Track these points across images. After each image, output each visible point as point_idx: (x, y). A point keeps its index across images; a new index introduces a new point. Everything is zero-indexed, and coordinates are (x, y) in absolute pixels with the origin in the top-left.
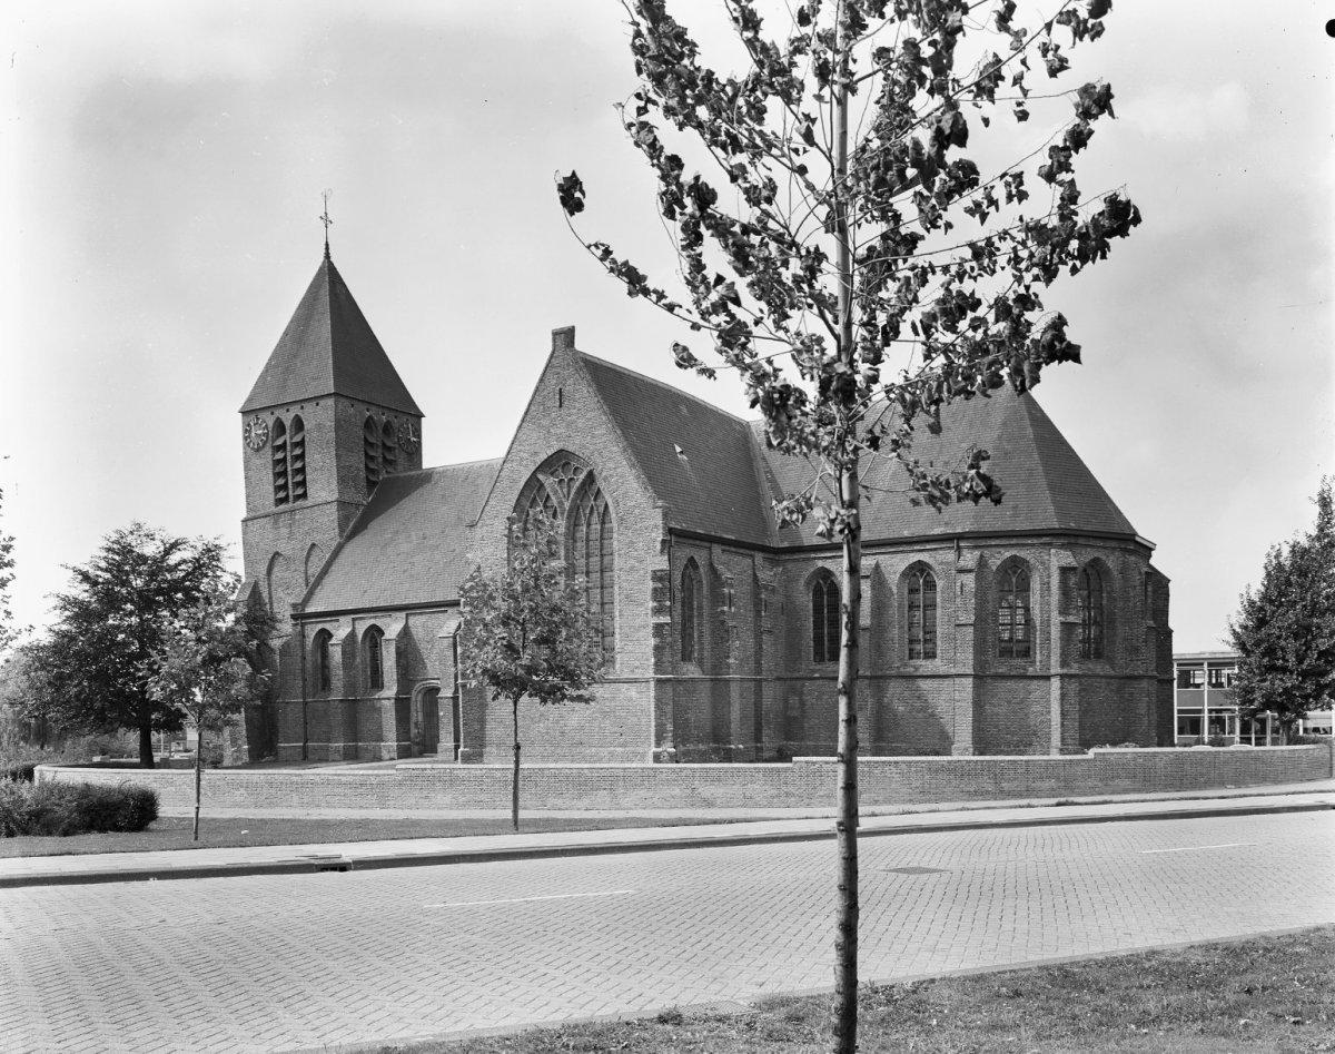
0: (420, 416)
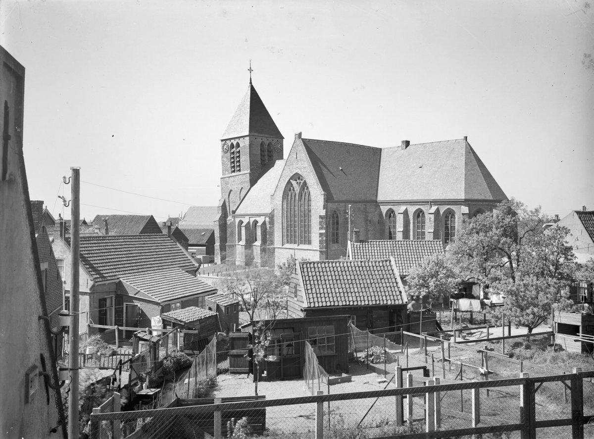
0: (283, 138)
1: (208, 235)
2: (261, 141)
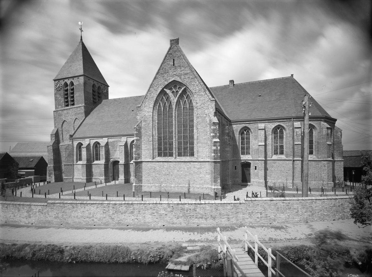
2: (93, 83)
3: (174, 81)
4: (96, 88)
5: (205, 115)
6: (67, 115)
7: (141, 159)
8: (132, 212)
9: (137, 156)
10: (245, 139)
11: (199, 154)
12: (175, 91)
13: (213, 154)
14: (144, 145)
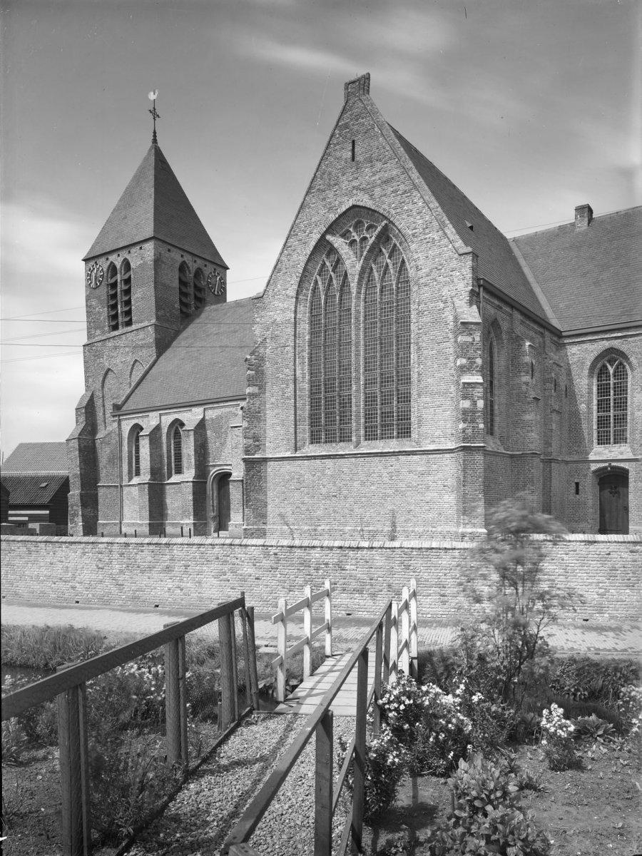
1: (55, 487)
2: (180, 260)
3: (354, 206)
4: (190, 273)
5: (442, 305)
6: (115, 354)
7: (264, 451)
8: (168, 569)
9: (251, 441)
10: (612, 392)
11: (423, 429)
12: (358, 240)
13: (461, 426)
14: (272, 409)
